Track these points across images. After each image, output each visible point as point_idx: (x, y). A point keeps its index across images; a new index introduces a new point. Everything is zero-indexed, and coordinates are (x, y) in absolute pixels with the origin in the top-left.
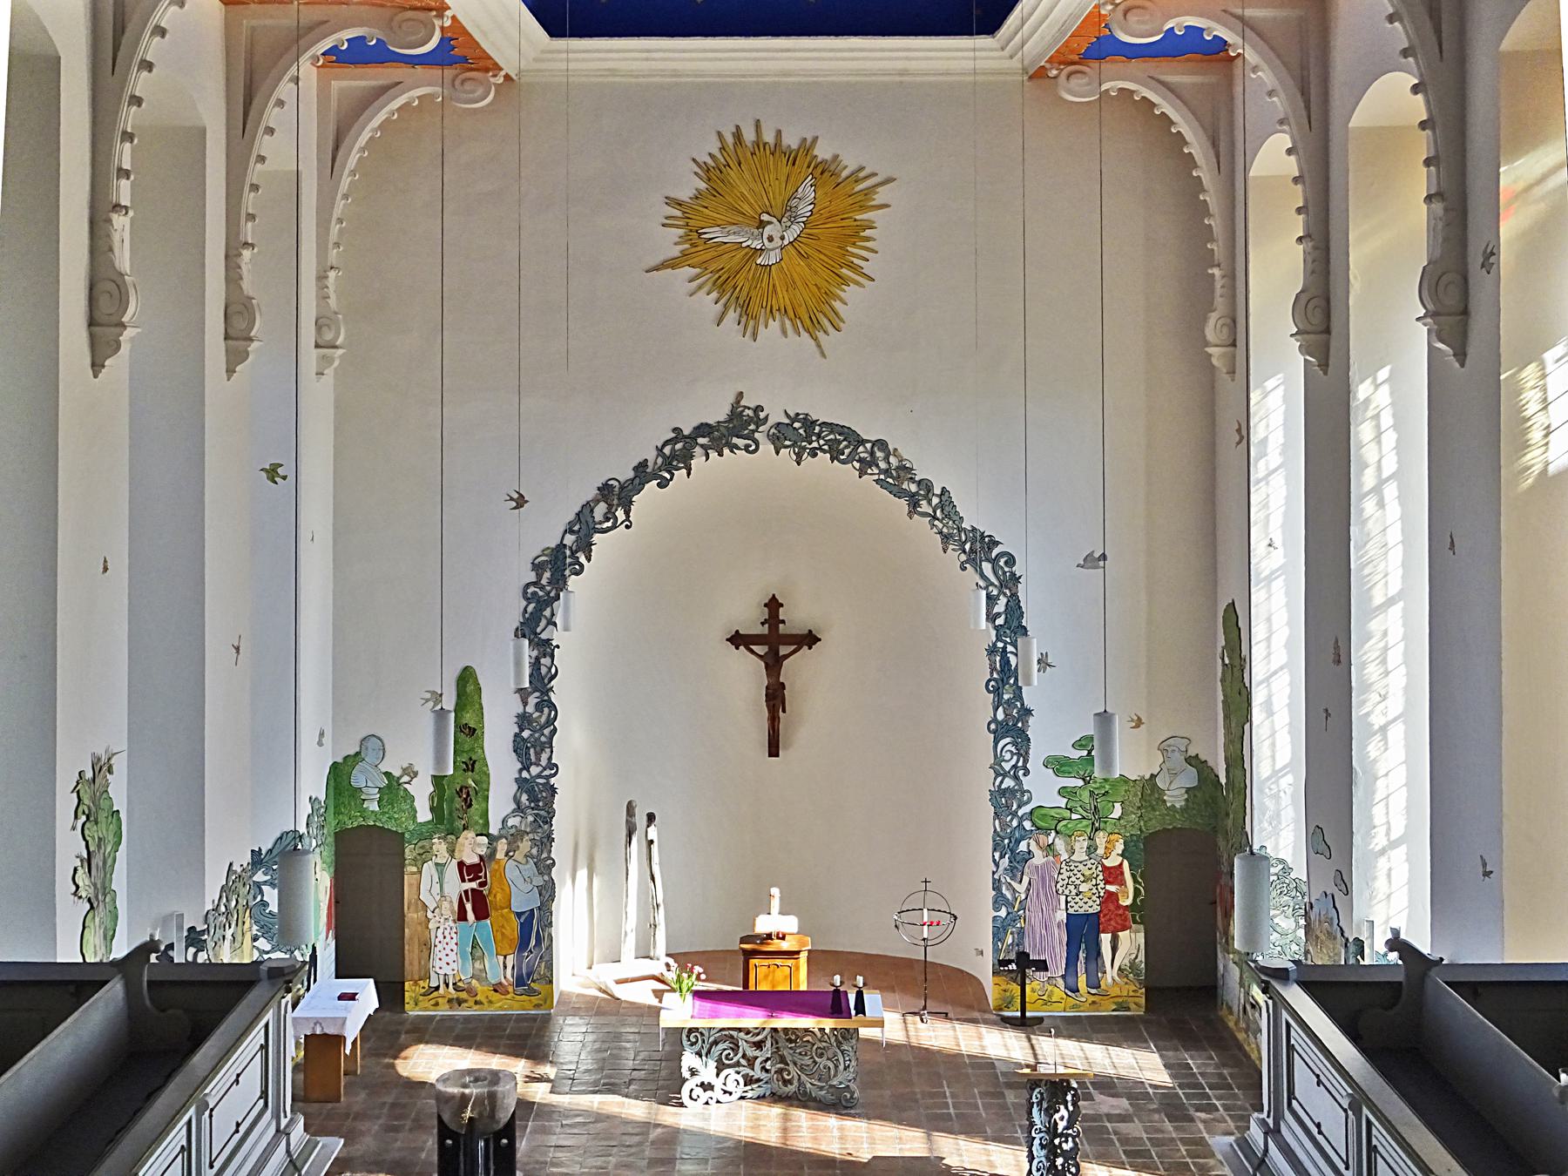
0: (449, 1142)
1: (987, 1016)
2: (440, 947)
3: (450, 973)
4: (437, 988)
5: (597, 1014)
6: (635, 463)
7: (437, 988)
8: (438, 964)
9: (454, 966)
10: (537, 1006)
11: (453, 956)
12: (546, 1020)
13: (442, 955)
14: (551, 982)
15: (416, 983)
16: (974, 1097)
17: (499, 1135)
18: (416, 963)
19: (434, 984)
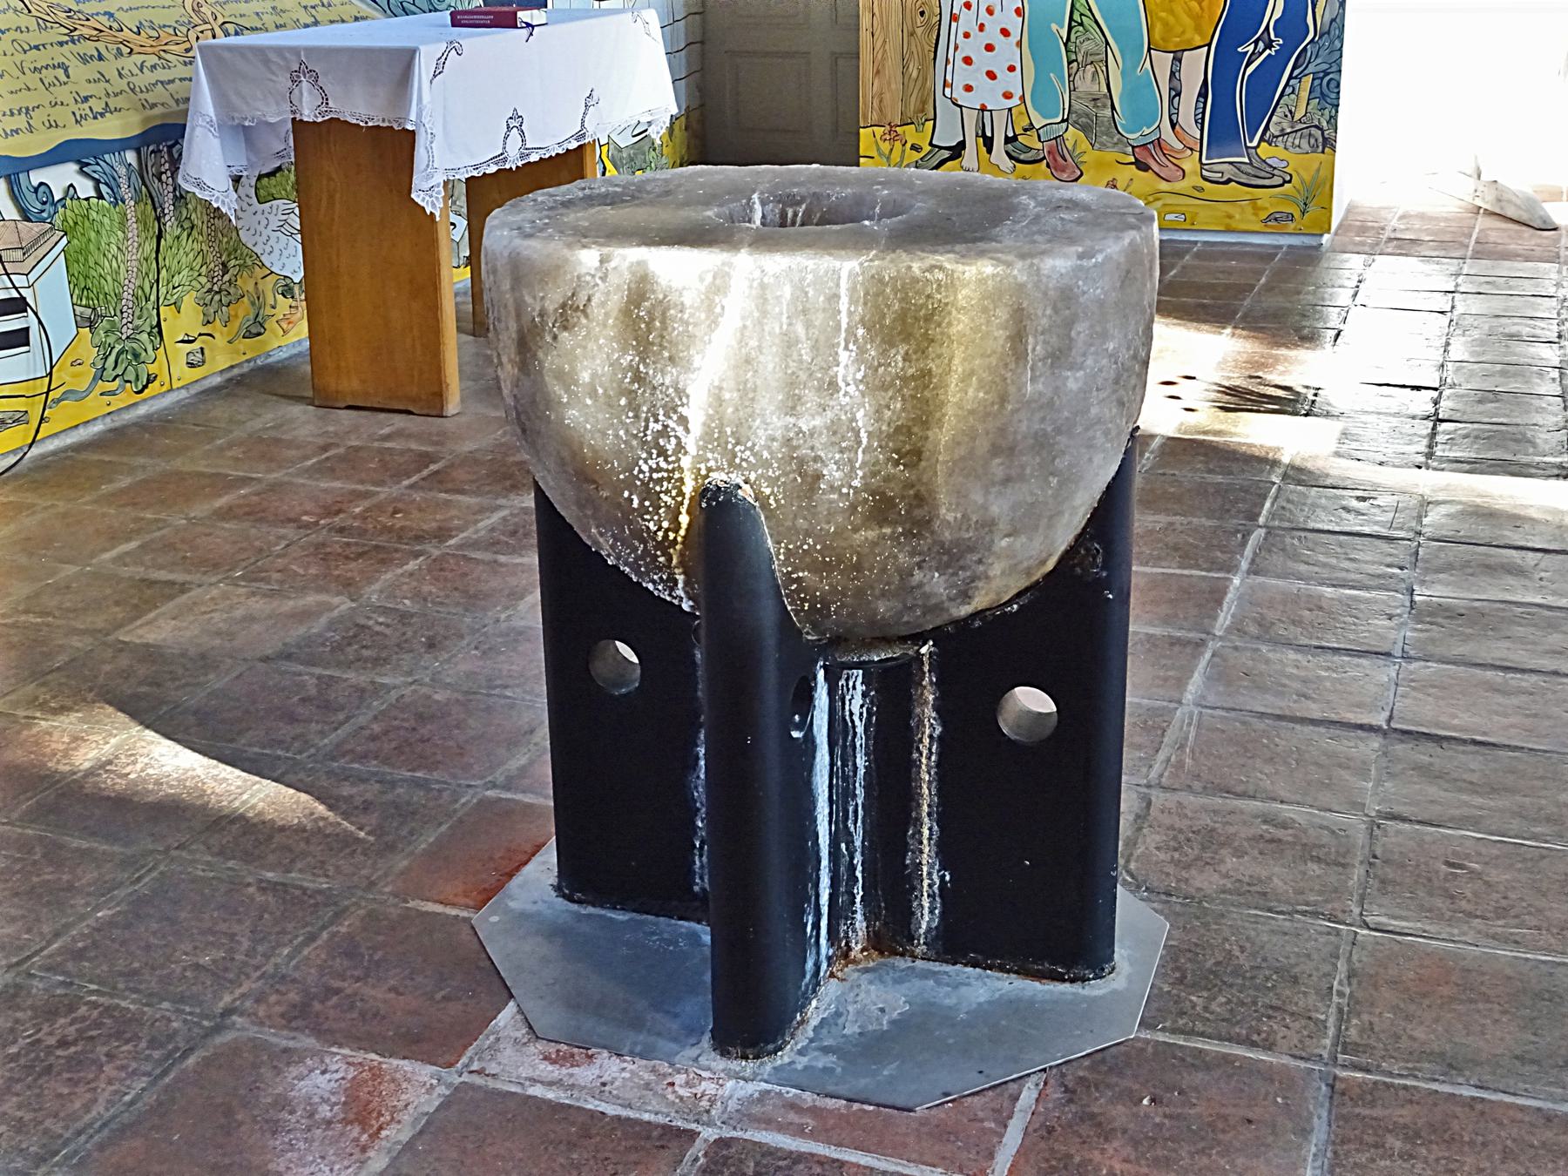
0: (1032, 700)
1: (824, 966)
2: (967, 21)
3: (996, 103)
4: (957, 151)
5: (1477, 256)
6: (1521, 181)
7: (957, 151)
8: (961, 74)
9: (1012, 82)
10: (1276, 220)
11: (1007, 51)
12: (1307, 259)
13: (973, 48)
14: (1329, 143)
15: (893, 136)
16: (368, 833)
17: (980, 654)
18: (892, 66)
19: (947, 139)
